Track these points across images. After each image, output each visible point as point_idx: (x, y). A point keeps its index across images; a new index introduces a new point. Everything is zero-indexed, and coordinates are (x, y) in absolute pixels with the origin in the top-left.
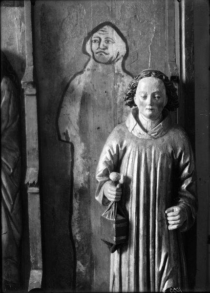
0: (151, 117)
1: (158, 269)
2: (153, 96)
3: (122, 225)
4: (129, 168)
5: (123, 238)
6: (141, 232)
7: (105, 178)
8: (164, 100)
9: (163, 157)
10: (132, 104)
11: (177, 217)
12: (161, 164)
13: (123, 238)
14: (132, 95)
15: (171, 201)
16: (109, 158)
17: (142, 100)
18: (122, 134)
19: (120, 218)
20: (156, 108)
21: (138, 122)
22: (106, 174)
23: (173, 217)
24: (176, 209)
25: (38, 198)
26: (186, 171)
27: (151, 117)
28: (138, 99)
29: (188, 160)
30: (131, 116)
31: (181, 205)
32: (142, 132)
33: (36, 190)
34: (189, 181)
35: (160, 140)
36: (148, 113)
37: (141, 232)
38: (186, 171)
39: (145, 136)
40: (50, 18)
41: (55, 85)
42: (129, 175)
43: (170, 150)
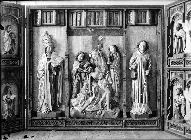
0: (143, 51)
1: (143, 84)
2: (144, 46)
3: (136, 74)
4: (137, 62)
5: (136, 77)
6: (140, 75)
7: (132, 64)
8: (146, 47)
9: (145, 59)
10: (138, 48)
11: (148, 72)
12: (145, 61)
13: (136, 77)
14: (138, 46)
15: (147, 69)
16: (133, 59)
17: (141, 47)
18: (136, 54)
19: (136, 72)
20: (144, 49)
21: (140, 52)
22: (132, 63)
23: (147, 72)
24: (148, 71)
25: (126, 82)
26: (150, 63)
27: (143, 51)
28: (140, 47)
29: (150, 60)
30: (138, 50)
31: (149, 70)
32: (141, 54)
33: (125, 80)
34: (151, 65)
35: (144, 56)
36: (142, 50)
37: (140, 75)
38: (150, 63)
39: (141, 55)
40: (129, 39)
41: (130, 55)
42: (138, 63)
43: (147, 58)
